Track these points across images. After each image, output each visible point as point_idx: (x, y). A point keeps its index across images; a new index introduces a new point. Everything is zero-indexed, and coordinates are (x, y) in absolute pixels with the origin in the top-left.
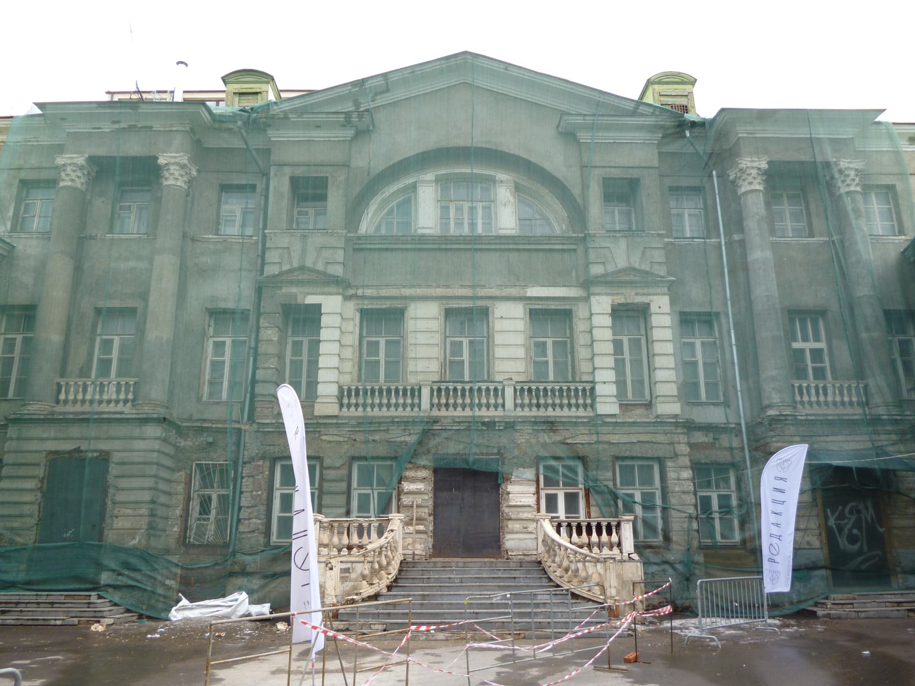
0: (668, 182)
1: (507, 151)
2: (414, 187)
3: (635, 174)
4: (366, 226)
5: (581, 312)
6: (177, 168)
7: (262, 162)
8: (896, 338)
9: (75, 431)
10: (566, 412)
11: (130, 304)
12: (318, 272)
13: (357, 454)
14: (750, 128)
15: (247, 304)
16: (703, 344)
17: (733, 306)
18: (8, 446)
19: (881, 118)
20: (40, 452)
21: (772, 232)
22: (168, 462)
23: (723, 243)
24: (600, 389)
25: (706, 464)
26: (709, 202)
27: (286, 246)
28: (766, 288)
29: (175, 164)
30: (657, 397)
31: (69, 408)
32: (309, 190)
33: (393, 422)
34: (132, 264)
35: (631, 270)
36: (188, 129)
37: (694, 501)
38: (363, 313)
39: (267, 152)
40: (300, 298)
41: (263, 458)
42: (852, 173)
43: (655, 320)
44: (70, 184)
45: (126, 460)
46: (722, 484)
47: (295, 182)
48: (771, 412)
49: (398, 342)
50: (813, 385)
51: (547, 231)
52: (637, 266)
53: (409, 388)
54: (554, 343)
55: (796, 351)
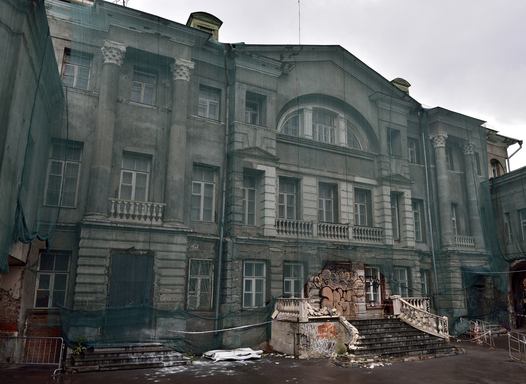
2: (301, 111)
5: (375, 192)
8: (215, 185)
11: (149, 152)
13: (287, 259)
19: (483, 125)
20: (106, 249)
27: (245, 132)
34: (148, 125)
35: (398, 175)
40: (254, 165)
44: (115, 62)
45: (165, 257)
53: (303, 223)
54: (205, 185)
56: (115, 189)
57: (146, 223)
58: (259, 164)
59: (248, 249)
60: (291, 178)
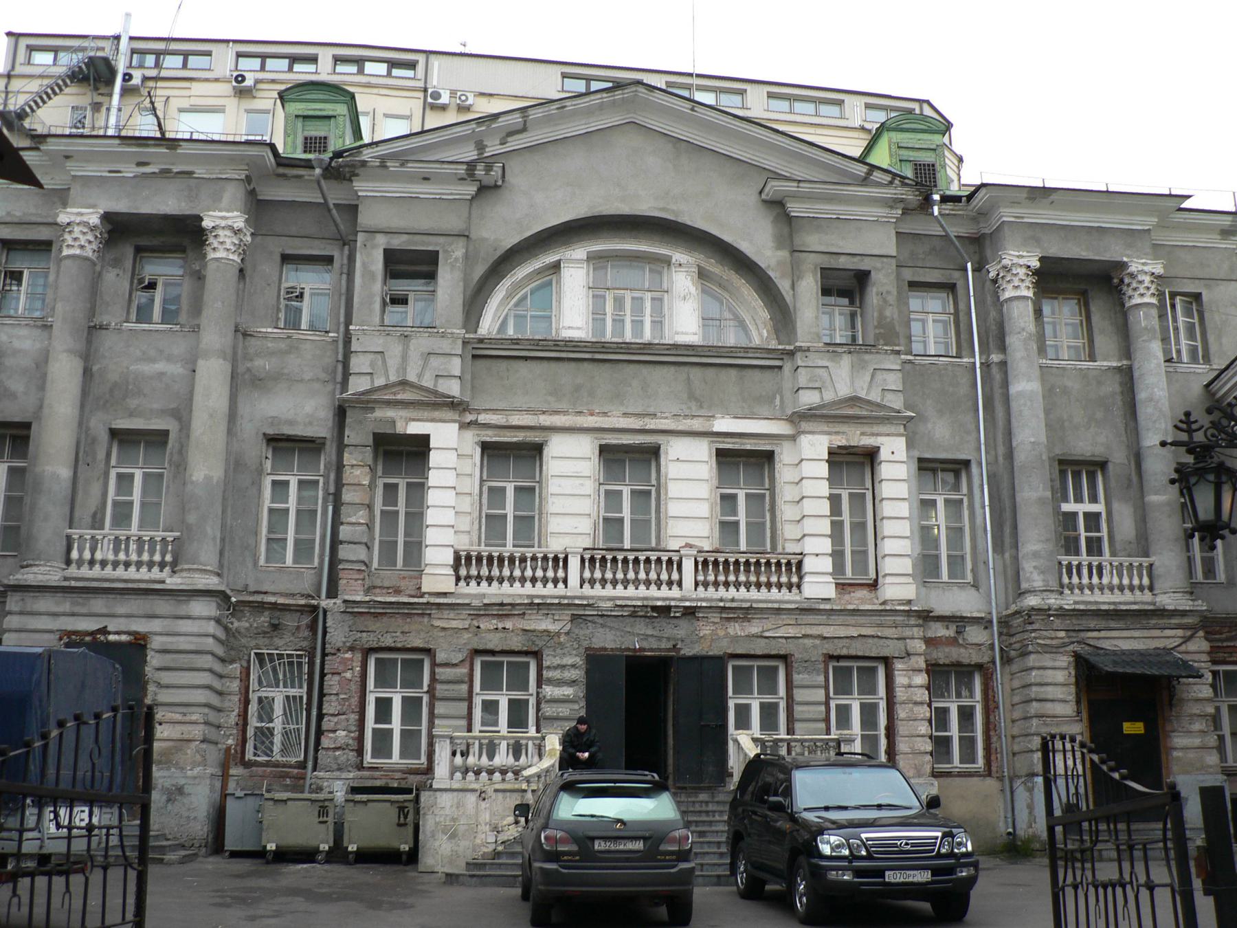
0: (908, 275)
1: (689, 223)
2: (556, 267)
3: (864, 265)
4: (488, 325)
5: (785, 456)
6: (228, 233)
7: (344, 224)
9: (98, 605)
10: (763, 594)
11: (157, 424)
12: (427, 390)
13: (481, 647)
14: (1018, 211)
15: (321, 428)
16: (946, 501)
17: (987, 453)
18: (12, 621)
21: (1042, 350)
22: (220, 651)
23: (978, 365)
24: (809, 564)
25: (944, 665)
26: (962, 306)
28: (1030, 433)
29: (225, 221)
30: (886, 575)
31: (85, 571)
32: (411, 266)
33: (531, 604)
34: (160, 366)
35: (854, 400)
36: (243, 177)
37: (928, 715)
38: (486, 447)
39: (352, 210)
41: (352, 649)
42: (1147, 279)
43: (885, 471)
44: (78, 252)
45: (169, 647)
46: (964, 692)
47: (391, 257)
48: (1032, 601)
49: (532, 489)
50: (1085, 563)
51: (744, 343)
52: (862, 394)
53: (551, 556)
55: (1066, 514)
56: (93, 509)
57: (137, 576)
58: (414, 420)
59: (378, 625)
60: (515, 443)
